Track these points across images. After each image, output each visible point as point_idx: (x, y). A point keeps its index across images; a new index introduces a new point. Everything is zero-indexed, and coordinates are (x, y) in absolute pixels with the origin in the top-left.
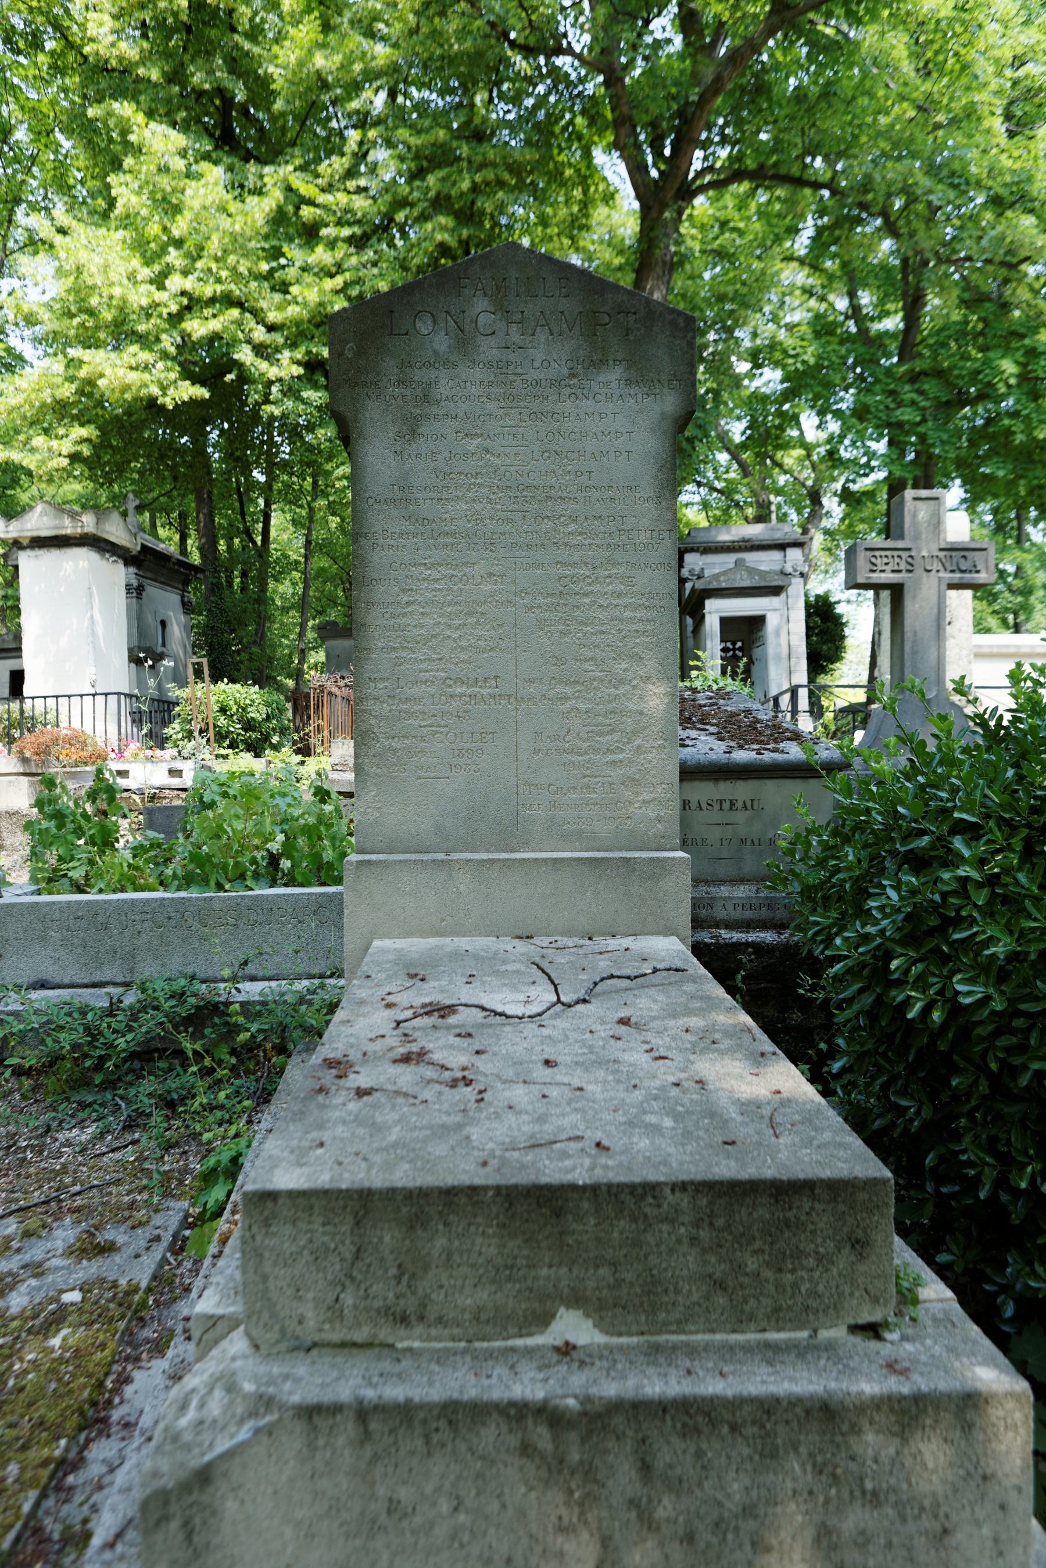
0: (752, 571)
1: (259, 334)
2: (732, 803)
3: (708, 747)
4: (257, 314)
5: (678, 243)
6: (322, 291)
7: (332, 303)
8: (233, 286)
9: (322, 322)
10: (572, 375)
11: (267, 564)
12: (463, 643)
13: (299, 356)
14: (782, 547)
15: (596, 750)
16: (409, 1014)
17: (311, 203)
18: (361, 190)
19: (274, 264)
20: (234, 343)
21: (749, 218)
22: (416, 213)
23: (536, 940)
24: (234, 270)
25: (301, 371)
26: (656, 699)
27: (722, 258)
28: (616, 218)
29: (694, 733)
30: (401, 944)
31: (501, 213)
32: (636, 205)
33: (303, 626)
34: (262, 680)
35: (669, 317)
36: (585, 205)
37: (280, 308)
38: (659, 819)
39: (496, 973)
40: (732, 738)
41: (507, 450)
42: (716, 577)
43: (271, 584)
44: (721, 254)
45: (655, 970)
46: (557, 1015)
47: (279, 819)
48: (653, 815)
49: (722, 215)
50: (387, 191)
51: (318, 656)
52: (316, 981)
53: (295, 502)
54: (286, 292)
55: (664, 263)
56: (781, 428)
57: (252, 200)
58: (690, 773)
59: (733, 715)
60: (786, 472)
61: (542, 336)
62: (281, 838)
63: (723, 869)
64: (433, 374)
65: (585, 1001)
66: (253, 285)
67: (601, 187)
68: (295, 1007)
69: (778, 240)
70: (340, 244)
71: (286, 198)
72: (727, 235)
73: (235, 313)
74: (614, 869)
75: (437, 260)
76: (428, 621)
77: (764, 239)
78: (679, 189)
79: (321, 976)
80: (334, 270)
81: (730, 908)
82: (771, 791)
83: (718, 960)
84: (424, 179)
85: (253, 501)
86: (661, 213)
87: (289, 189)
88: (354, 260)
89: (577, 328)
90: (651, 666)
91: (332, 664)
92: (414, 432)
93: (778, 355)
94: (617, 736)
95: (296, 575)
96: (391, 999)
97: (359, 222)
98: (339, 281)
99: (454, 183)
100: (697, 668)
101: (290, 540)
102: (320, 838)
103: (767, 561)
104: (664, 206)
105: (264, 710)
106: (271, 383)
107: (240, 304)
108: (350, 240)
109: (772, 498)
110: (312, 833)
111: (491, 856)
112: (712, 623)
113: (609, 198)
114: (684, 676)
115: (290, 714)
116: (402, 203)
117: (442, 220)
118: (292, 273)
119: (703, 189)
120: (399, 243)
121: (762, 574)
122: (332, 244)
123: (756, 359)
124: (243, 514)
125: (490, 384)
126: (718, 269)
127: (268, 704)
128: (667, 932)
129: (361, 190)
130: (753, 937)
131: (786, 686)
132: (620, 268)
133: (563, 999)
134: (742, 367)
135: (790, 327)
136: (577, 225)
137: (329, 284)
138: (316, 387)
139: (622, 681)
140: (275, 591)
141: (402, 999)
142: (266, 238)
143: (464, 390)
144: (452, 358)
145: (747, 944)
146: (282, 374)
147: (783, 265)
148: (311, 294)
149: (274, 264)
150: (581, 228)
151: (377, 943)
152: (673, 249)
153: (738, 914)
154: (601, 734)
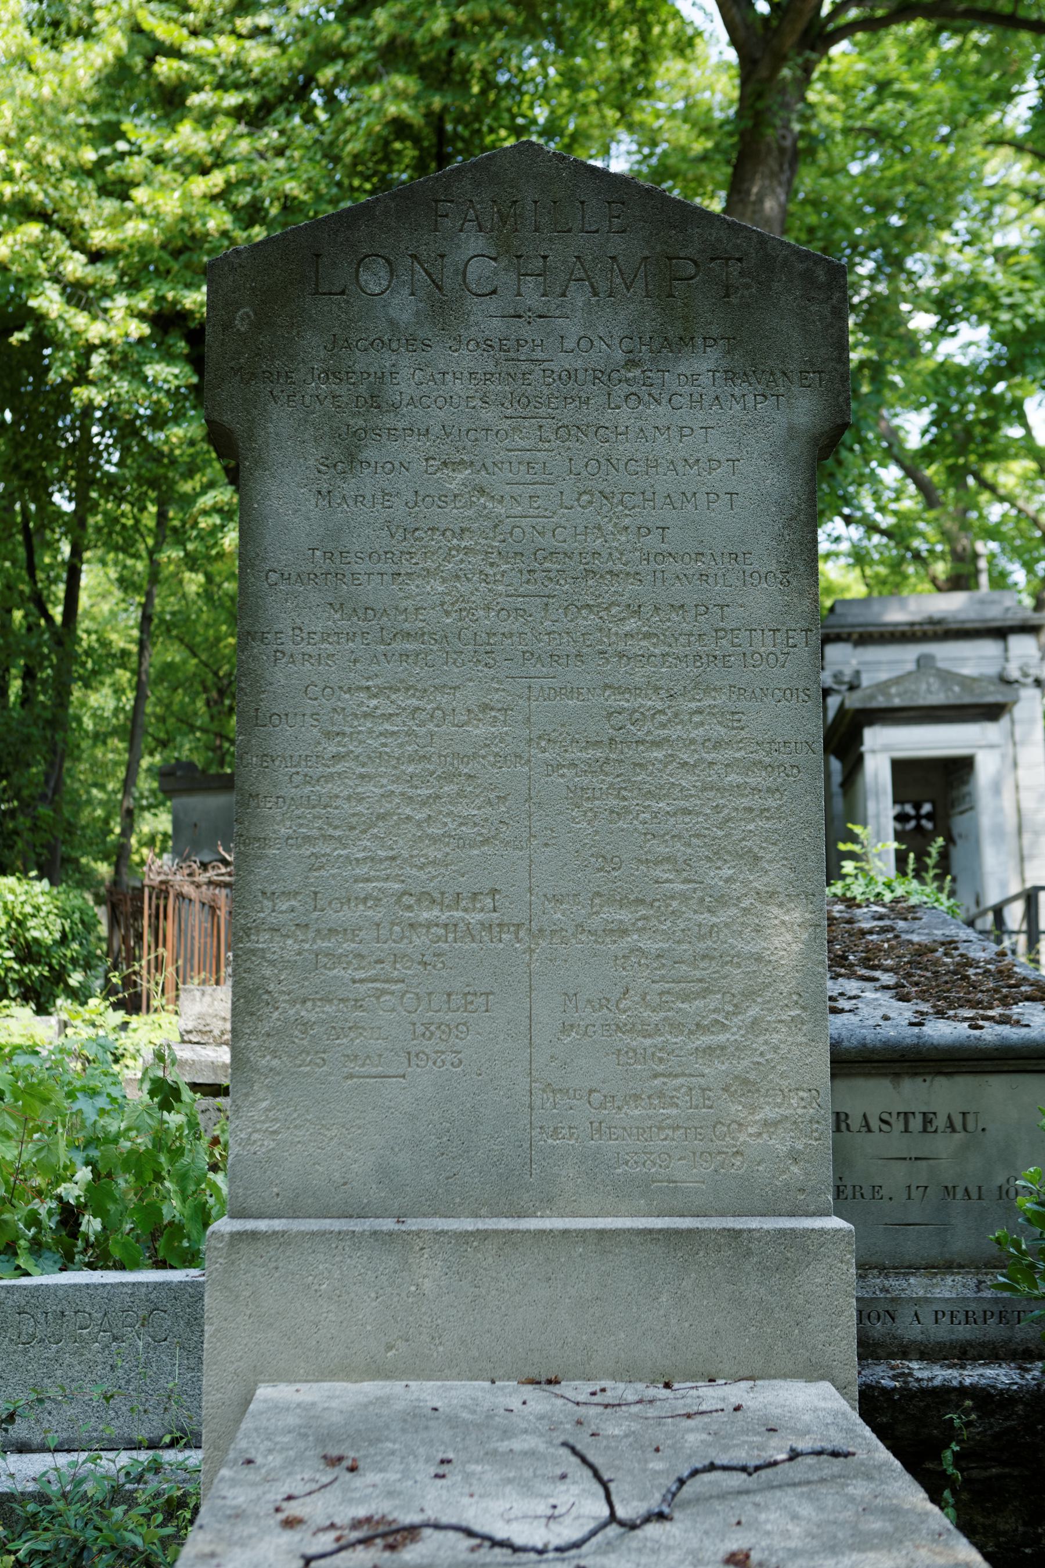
0: (947, 677)
1: (75, 266)
2: (927, 1119)
3: (879, 1013)
4: (74, 234)
5: (805, 119)
6: (187, 197)
7: (203, 217)
8: (33, 187)
9: (183, 249)
10: (632, 363)
11: (74, 657)
12: (434, 830)
13: (143, 305)
14: (1000, 633)
15: (676, 1027)
16: (326, 1541)
17: (174, 52)
18: (257, 32)
19: (106, 151)
20: (29, 281)
21: (923, 77)
22: (353, 68)
23: (566, 1388)
24: (36, 161)
25: (146, 330)
26: (787, 937)
27: (881, 142)
28: (696, 75)
29: (852, 986)
30: (310, 1393)
31: (498, 67)
32: (732, 55)
33: (132, 768)
34: (53, 867)
35: (801, 267)
36: (644, 57)
37: (113, 223)
38: (795, 1156)
39: (492, 1456)
40: (923, 996)
41: (517, 490)
42: (883, 687)
43: (77, 692)
44: (878, 135)
45: (794, 1455)
46: (609, 1547)
47: (81, 1137)
48: (782, 1149)
49: (880, 72)
50: (305, 33)
51: (158, 822)
52: (144, 1456)
53: (127, 547)
54: (125, 197)
55: (782, 150)
56: (992, 425)
57: (74, 48)
58: (851, 1062)
59: (923, 950)
60: (1002, 499)
61: (578, 296)
62: (84, 1174)
63: (914, 1245)
64: (388, 360)
65: (661, 1516)
66: (69, 185)
67: (671, 27)
68: (102, 1506)
69: (977, 113)
70: (221, 119)
71: (132, 45)
72: (889, 104)
73: (34, 230)
74: (710, 1254)
75: (387, 143)
76: (370, 789)
77: (953, 112)
78: (806, 32)
79: (153, 1445)
80: (209, 161)
81: (927, 1318)
82: (999, 1096)
83: (904, 1422)
84: (368, 16)
85: (52, 547)
86: (776, 69)
87: (137, 29)
88: (243, 146)
89: (639, 283)
90: (774, 874)
91: (184, 840)
92: (352, 459)
93: (980, 302)
94: (714, 1000)
95: (123, 676)
96: (293, 1509)
97: (256, 83)
98: (217, 179)
99: (421, 22)
100: (852, 856)
101: (113, 614)
102: (158, 1177)
103: (973, 659)
104: (780, 60)
105: (57, 925)
106: (91, 348)
107: (43, 216)
108: (239, 113)
109: (980, 547)
110: (144, 1167)
111: (481, 1224)
112: (877, 770)
113: (685, 45)
114: (833, 873)
115: (103, 930)
116: (330, 53)
117: (399, 81)
118: (136, 166)
119: (847, 31)
120: (322, 116)
121: (966, 682)
122: (206, 119)
123: (946, 308)
124: (31, 568)
125: (488, 376)
126: (874, 158)
127: (64, 914)
128: (812, 1372)
129: (257, 32)
130: (972, 1375)
131: (1015, 888)
132: (705, 158)
133: (621, 1512)
134: (923, 321)
135: (1003, 255)
136: (627, 91)
137: (200, 185)
138: (169, 357)
139: (722, 901)
140: (83, 704)
141: (315, 1509)
142: (94, 107)
143: (439, 385)
144: (420, 334)
145: (963, 1391)
146: (113, 334)
147: (985, 154)
148: (166, 201)
149: (106, 151)
150: (637, 94)
151: (264, 1392)
152: (797, 127)
153: (942, 1332)
154: (686, 998)
